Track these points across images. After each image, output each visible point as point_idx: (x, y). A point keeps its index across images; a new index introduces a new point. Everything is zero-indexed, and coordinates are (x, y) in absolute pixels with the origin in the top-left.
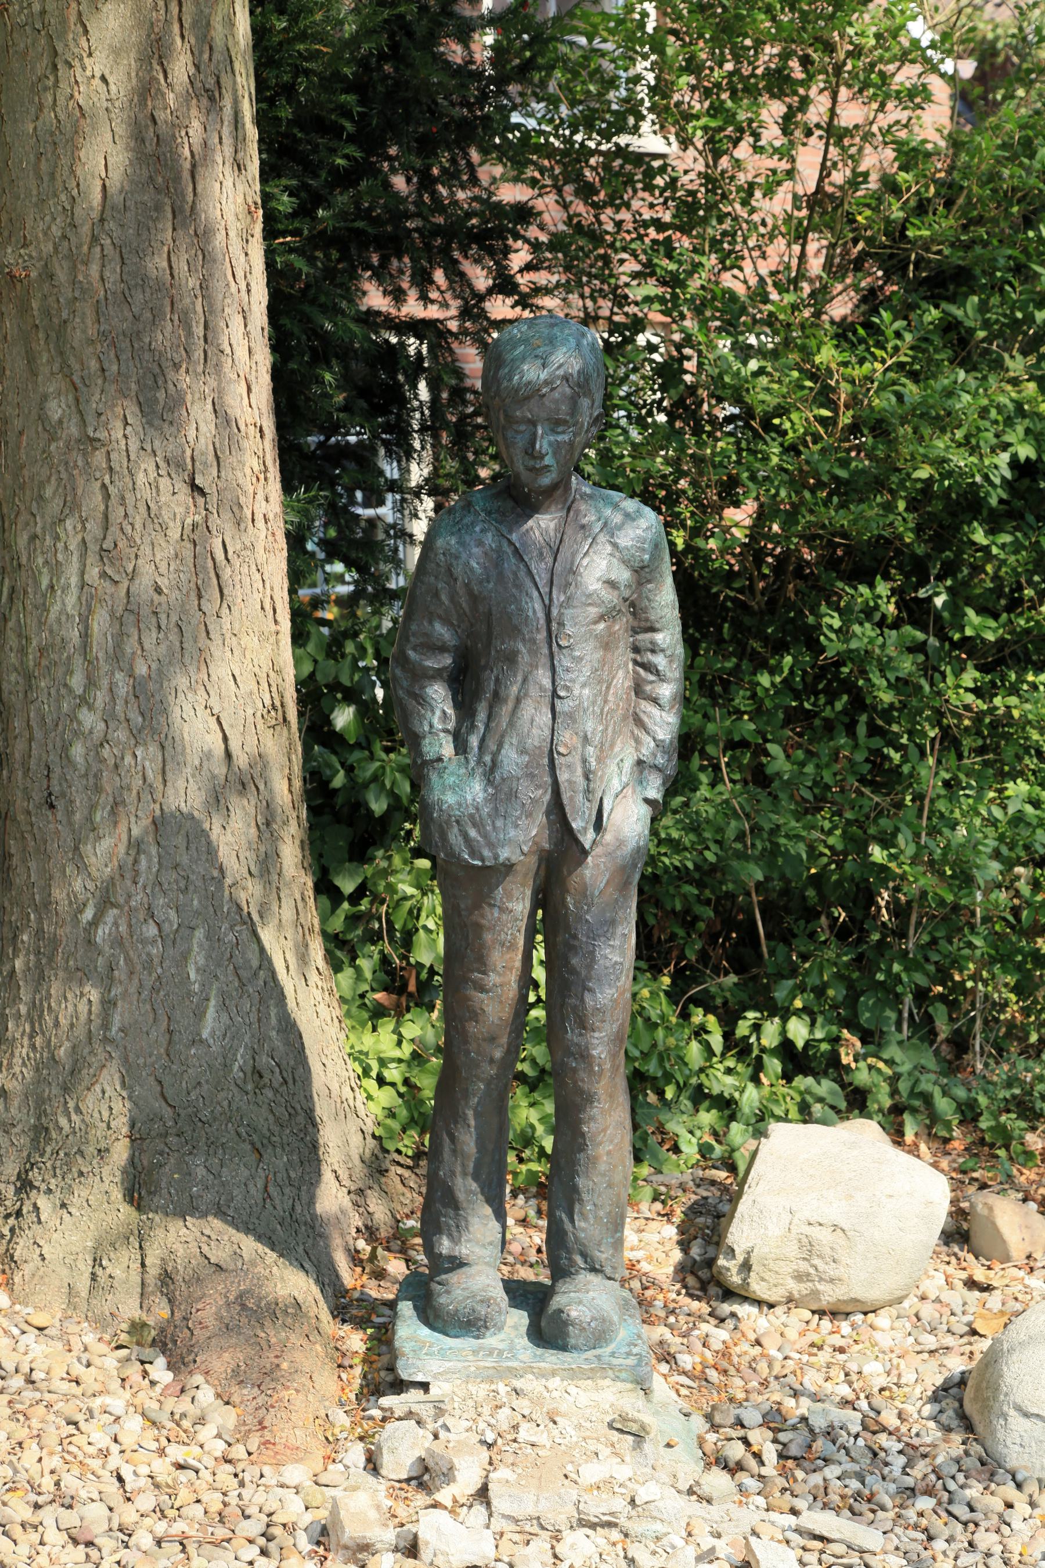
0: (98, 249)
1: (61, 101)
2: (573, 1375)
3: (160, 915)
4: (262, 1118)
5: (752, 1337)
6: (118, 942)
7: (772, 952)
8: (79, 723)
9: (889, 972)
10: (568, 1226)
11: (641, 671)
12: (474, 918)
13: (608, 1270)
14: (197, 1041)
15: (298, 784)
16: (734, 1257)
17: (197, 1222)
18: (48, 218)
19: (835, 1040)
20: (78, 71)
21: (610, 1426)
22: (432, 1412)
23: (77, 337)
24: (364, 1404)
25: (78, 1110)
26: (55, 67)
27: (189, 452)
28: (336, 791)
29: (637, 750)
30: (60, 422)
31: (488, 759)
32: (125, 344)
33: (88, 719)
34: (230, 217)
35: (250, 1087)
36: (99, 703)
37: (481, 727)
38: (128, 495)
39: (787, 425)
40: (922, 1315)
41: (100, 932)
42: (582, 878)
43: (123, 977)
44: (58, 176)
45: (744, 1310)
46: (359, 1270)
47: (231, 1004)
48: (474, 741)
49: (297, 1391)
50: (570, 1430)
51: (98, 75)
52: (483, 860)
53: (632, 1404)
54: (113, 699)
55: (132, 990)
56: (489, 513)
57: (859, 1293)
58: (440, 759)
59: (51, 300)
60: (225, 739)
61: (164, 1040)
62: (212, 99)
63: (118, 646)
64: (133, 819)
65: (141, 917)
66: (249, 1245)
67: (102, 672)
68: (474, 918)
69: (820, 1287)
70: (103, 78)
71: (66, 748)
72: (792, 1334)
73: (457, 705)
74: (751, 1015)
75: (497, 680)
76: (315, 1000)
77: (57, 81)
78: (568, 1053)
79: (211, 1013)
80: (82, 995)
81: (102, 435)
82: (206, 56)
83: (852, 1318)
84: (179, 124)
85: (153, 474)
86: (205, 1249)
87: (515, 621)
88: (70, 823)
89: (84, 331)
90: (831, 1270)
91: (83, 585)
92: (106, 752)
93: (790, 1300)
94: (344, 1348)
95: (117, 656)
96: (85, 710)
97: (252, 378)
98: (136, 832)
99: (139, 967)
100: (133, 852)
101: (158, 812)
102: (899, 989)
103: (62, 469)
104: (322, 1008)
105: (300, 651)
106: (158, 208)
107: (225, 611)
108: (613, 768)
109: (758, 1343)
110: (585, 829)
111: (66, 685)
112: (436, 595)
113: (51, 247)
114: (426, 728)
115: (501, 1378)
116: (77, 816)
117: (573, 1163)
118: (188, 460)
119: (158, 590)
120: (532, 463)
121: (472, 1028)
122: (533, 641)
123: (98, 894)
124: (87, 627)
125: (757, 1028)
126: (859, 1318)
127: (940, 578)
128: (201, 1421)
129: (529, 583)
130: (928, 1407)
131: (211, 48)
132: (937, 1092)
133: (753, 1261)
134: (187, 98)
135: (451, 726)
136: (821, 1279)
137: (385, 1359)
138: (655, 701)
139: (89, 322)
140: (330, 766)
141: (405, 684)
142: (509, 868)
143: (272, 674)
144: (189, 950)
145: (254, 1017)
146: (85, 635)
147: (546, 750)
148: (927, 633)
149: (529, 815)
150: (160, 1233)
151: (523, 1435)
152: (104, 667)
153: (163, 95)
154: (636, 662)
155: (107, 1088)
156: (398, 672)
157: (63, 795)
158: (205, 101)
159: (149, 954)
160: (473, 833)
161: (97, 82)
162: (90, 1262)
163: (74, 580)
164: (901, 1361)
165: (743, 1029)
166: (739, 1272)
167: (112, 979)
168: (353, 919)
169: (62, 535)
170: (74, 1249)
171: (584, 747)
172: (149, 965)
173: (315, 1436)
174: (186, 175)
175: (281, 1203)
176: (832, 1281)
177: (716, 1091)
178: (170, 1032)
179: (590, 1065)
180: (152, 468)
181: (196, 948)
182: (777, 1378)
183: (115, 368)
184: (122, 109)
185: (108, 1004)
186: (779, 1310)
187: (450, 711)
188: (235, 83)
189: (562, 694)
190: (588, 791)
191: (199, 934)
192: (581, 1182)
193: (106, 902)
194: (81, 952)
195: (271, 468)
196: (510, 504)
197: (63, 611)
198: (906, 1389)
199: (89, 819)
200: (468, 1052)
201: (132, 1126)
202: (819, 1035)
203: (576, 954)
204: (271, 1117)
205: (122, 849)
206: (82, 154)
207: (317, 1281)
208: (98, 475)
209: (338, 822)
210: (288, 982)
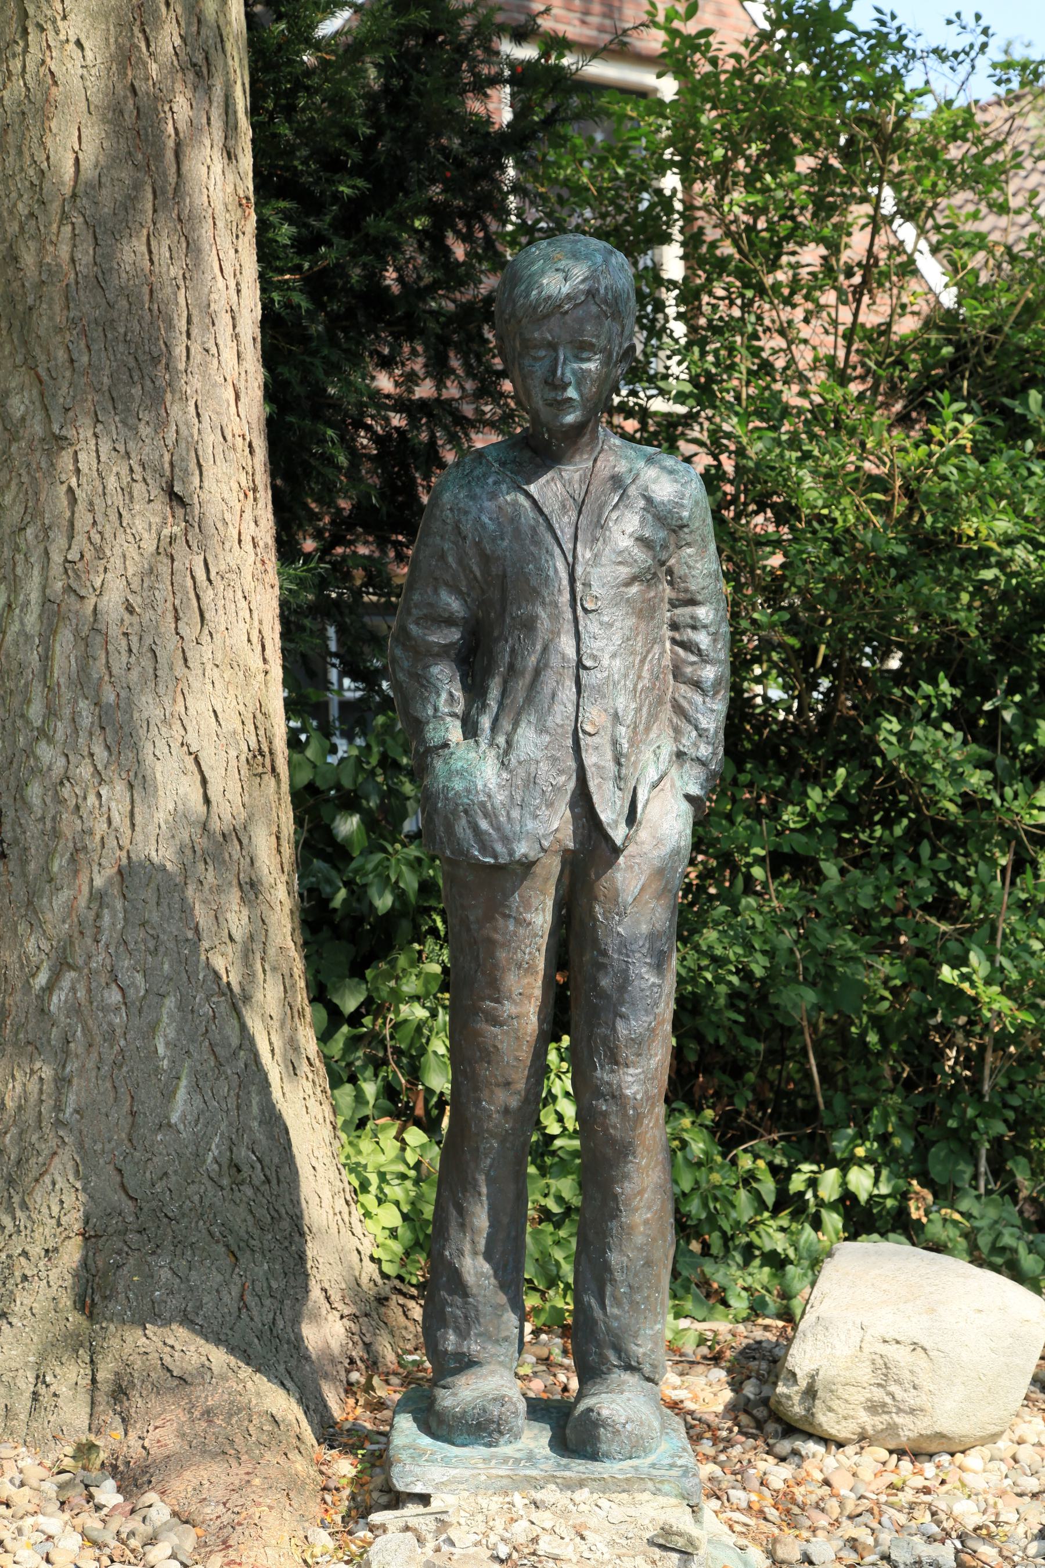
0: (69, 228)
1: (31, 67)
2: (604, 1486)
3: (124, 979)
4: (239, 1219)
5: (820, 1477)
6: (75, 1010)
7: (828, 1104)
8: (37, 759)
9: (962, 1117)
10: (598, 1313)
11: (681, 651)
12: (485, 932)
13: (647, 1369)
14: (164, 1125)
15: (287, 850)
16: (795, 1382)
17: (159, 1331)
18: (14, 195)
19: (904, 1196)
20: (51, 34)
21: (651, 1543)
22: (433, 1526)
23: (42, 325)
24: (351, 1525)
25: (24, 1206)
26: (25, 32)
27: (167, 457)
28: (335, 910)
29: (676, 740)
30: (23, 419)
31: (501, 740)
32: (98, 334)
33: (45, 752)
34: (219, 207)
35: (225, 1182)
36: (60, 735)
37: (493, 705)
38: (97, 501)
39: (837, 514)
40: (1019, 1457)
41: (55, 999)
42: (612, 880)
43: (80, 1050)
44: (25, 149)
45: (811, 1447)
46: (351, 1401)
47: (207, 1087)
48: (486, 722)
49: (271, 1508)
50: (602, 1547)
51: (73, 39)
52: (495, 856)
53: (681, 1519)
54: (76, 731)
55: (90, 1065)
56: (503, 464)
57: (945, 1426)
58: (446, 745)
59: (16, 285)
60: (204, 782)
61: (125, 1123)
62: (198, 74)
63: (84, 669)
64: (96, 868)
65: (103, 981)
66: (219, 1357)
67: (64, 701)
69: (899, 1420)
70: (79, 44)
71: (21, 787)
72: (866, 1473)
73: (466, 688)
74: (806, 1167)
75: (513, 650)
76: (306, 1111)
77: (27, 46)
78: (598, 1094)
79: (181, 1094)
80: (32, 1072)
81: (71, 433)
82: (194, 29)
83: (937, 1459)
84: (161, 98)
85: (126, 479)
86: (167, 1360)
87: (533, 582)
88: (24, 875)
89: (51, 319)
90: (910, 1399)
91: (46, 600)
92: (66, 792)
93: (863, 1437)
94: (330, 1472)
95: (82, 680)
96: (43, 744)
97: (241, 385)
98: (99, 882)
99: (99, 1039)
100: (95, 906)
101: (125, 861)
102: (974, 1136)
103: (23, 471)
104: (312, 1103)
105: (297, 757)
106: (137, 186)
107: (205, 638)
108: (648, 755)
109: (827, 1483)
110: (616, 822)
111: (22, 716)
112: (442, 557)
113: (16, 227)
114: (430, 712)
115: (517, 1489)
116: (32, 866)
117: (603, 1234)
118: (167, 466)
119: (130, 609)
120: (552, 395)
121: (484, 1071)
122: (555, 605)
123: (53, 955)
124: (47, 650)
125: (813, 1183)
126: (945, 1459)
127: (1010, 691)
128: (152, 1540)
129: (549, 538)
130: (1035, 1544)
131: (199, 21)
132: (1022, 1250)
133: (819, 1385)
134: (173, 71)
135: (459, 709)
136: (899, 1410)
137: (379, 1480)
138: (697, 685)
139: (57, 308)
140: (329, 882)
141: (406, 664)
142: (527, 866)
143: (259, 715)
144: (158, 1021)
145: (232, 1102)
146: (46, 658)
147: (570, 729)
148: (995, 751)
149: (550, 805)
150: (115, 1342)
151: (543, 1547)
152: (67, 694)
153: (145, 64)
154: (674, 641)
155: (59, 1179)
156: (398, 652)
157: (16, 841)
158: (191, 76)
159: (110, 1024)
160: (484, 825)
161: (71, 47)
162: (32, 1380)
163: (35, 596)
164: (1000, 1502)
165: (797, 1183)
166: (802, 1401)
167: (67, 1052)
168: (354, 1042)
169: (23, 546)
170: (14, 1365)
171: (614, 726)
172: (110, 1036)
173: (291, 1556)
174: (170, 155)
175: (261, 1315)
176: (912, 1411)
177: (767, 1248)
178: (133, 1114)
179: (624, 1108)
180: (124, 471)
181: (165, 1019)
182: (850, 1518)
183: (85, 359)
184: (99, 77)
185: (62, 1082)
186: (850, 1450)
187: (458, 694)
188: (226, 64)
189: (588, 663)
190: (619, 778)
191: (170, 1003)
192: (614, 1258)
193: (62, 964)
194: (33, 1022)
195: (261, 487)
196: (527, 454)
197: (22, 632)
198: (1006, 1528)
199: (46, 869)
200: (480, 1101)
201: (87, 1222)
202: (884, 1189)
203: (607, 974)
204: (249, 1217)
205: (82, 901)
206: (53, 124)
207: (300, 1401)
208: (64, 477)
209: (339, 938)
210: (274, 1070)
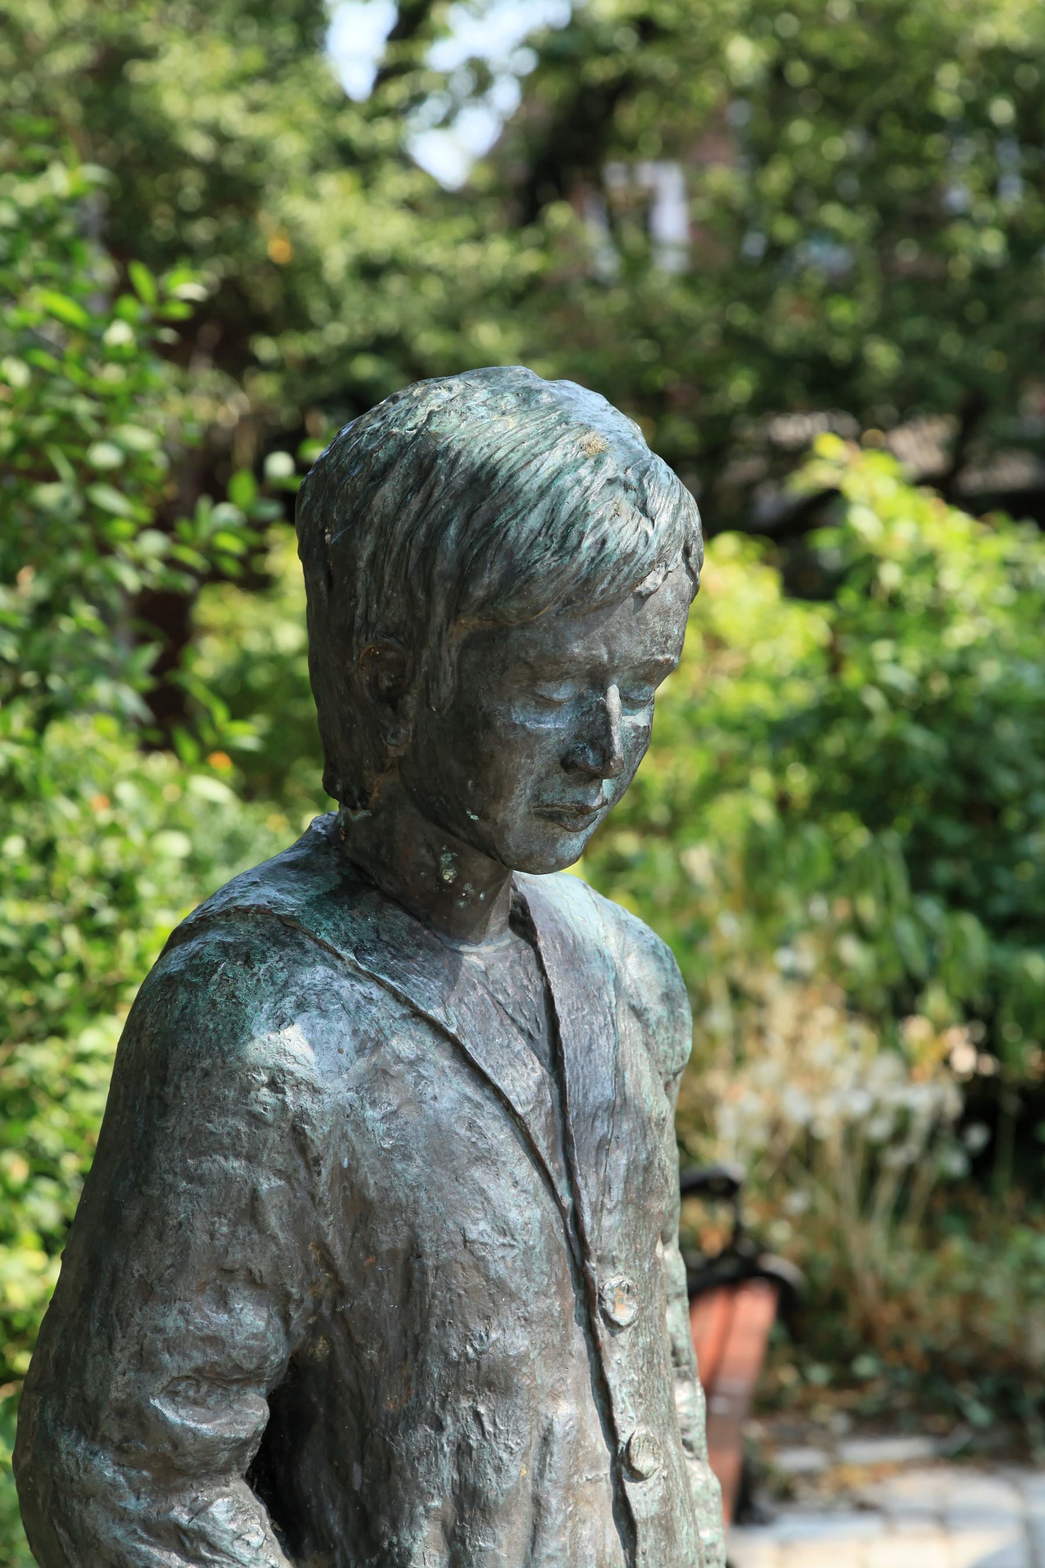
75: (463, 1450)
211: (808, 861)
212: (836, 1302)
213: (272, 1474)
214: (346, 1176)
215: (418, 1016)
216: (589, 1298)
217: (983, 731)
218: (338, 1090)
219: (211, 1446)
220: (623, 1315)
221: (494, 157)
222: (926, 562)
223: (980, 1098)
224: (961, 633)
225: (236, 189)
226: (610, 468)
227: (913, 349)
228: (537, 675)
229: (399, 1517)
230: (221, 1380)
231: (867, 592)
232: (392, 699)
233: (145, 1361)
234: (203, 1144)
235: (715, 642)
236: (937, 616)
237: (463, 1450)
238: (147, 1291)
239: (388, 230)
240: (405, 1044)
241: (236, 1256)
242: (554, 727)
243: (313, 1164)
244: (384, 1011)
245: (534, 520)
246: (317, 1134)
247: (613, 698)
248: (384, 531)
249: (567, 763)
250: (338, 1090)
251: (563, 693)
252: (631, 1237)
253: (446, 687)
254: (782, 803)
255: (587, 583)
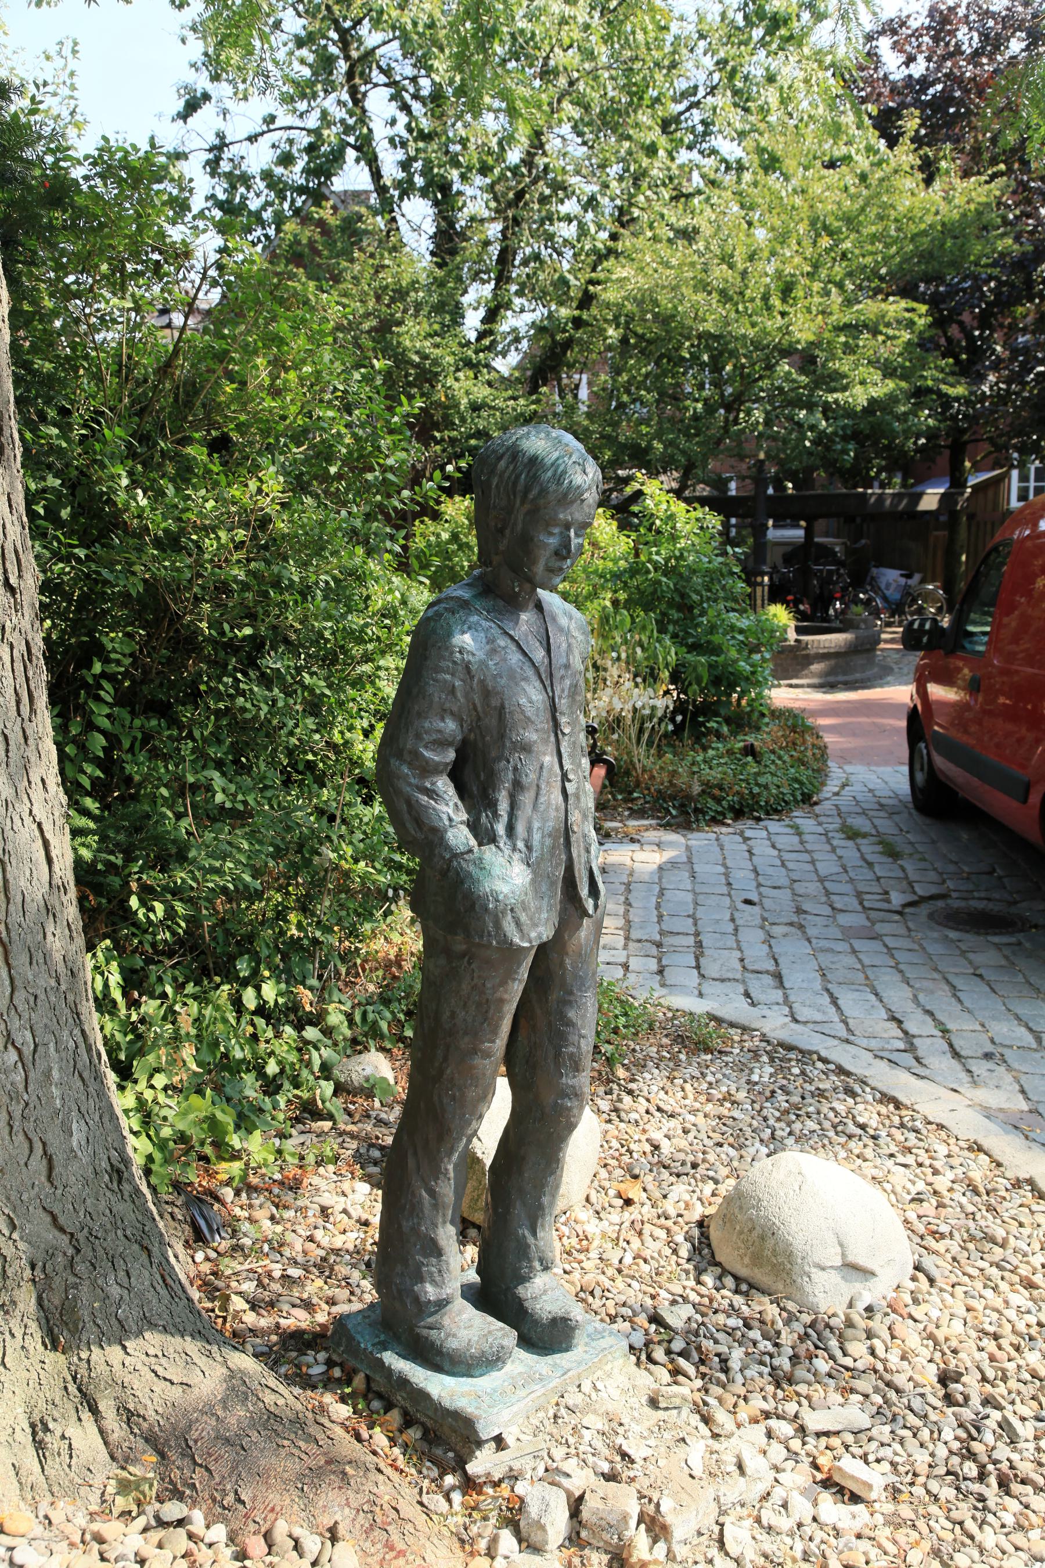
10: (531, 1240)
12: (498, 995)
31: (520, 845)
68: (498, 995)
75: (515, 769)
211: (622, 621)
212: (627, 773)
213: (456, 775)
214: (482, 682)
215: (506, 633)
216: (556, 725)
217: (689, 580)
218: (480, 655)
219: (438, 764)
220: (567, 731)
221: (519, 367)
222: (671, 517)
223: (680, 707)
224: (682, 543)
225: (427, 376)
226: (574, 458)
227: (668, 444)
228: (549, 524)
229: (495, 789)
230: (441, 744)
231: (650, 530)
232: (501, 531)
233: (418, 737)
234: (438, 670)
235: (595, 544)
236: (674, 538)
237: (515, 769)
238: (419, 715)
239: (482, 392)
240: (502, 642)
241: (447, 705)
242: (553, 541)
243: (472, 677)
244: (495, 631)
245: (549, 474)
246: (473, 668)
247: (572, 533)
248: (501, 476)
249: (557, 553)
250: (480, 655)
251: (556, 531)
252: (570, 707)
253: (520, 526)
254: (615, 603)
255: (565, 495)
